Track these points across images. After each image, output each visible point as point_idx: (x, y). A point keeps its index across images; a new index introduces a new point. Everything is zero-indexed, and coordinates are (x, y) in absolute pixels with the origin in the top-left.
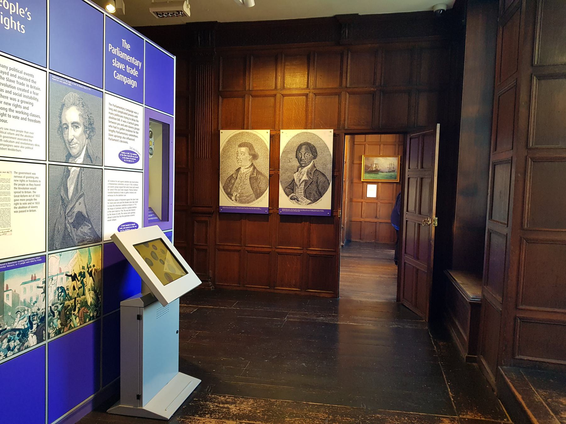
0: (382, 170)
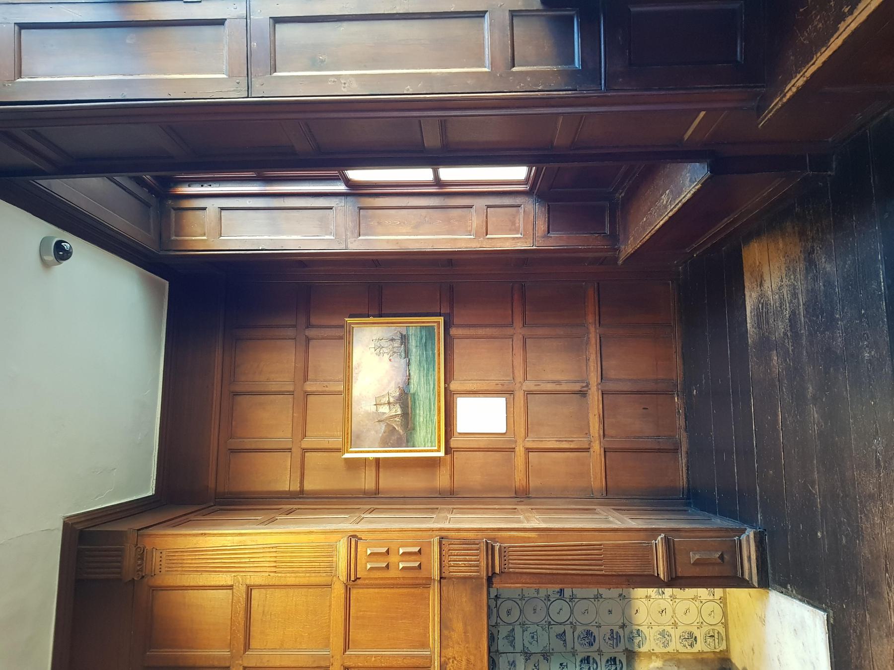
0: (400, 379)
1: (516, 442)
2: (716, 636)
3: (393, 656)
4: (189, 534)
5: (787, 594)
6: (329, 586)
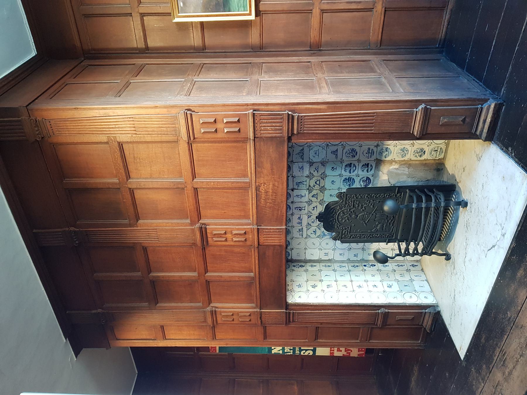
1: (313, 4)
2: (439, 151)
3: (225, 182)
4: (67, 109)
5: (506, 152)
6: (176, 142)
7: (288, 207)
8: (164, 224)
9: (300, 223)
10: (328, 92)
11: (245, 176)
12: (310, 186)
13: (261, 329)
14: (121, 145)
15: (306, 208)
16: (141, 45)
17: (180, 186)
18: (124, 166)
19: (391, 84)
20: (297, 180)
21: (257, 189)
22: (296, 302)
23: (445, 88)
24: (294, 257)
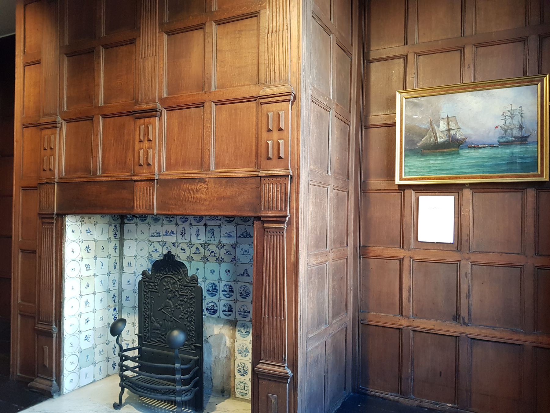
0: (474, 138)
2: (245, 392)
3: (210, 141)
6: (258, 83)
7: (185, 218)
8: (162, 65)
9: (166, 234)
10: (311, 263)
11: (217, 165)
12: (209, 244)
13: (33, 183)
14: (255, 15)
15: (184, 241)
16: (373, 55)
17: (206, 85)
18: (230, 18)
19: (317, 337)
20: (216, 230)
21: (202, 180)
22: (67, 227)
23: (311, 398)
24: (126, 227)
